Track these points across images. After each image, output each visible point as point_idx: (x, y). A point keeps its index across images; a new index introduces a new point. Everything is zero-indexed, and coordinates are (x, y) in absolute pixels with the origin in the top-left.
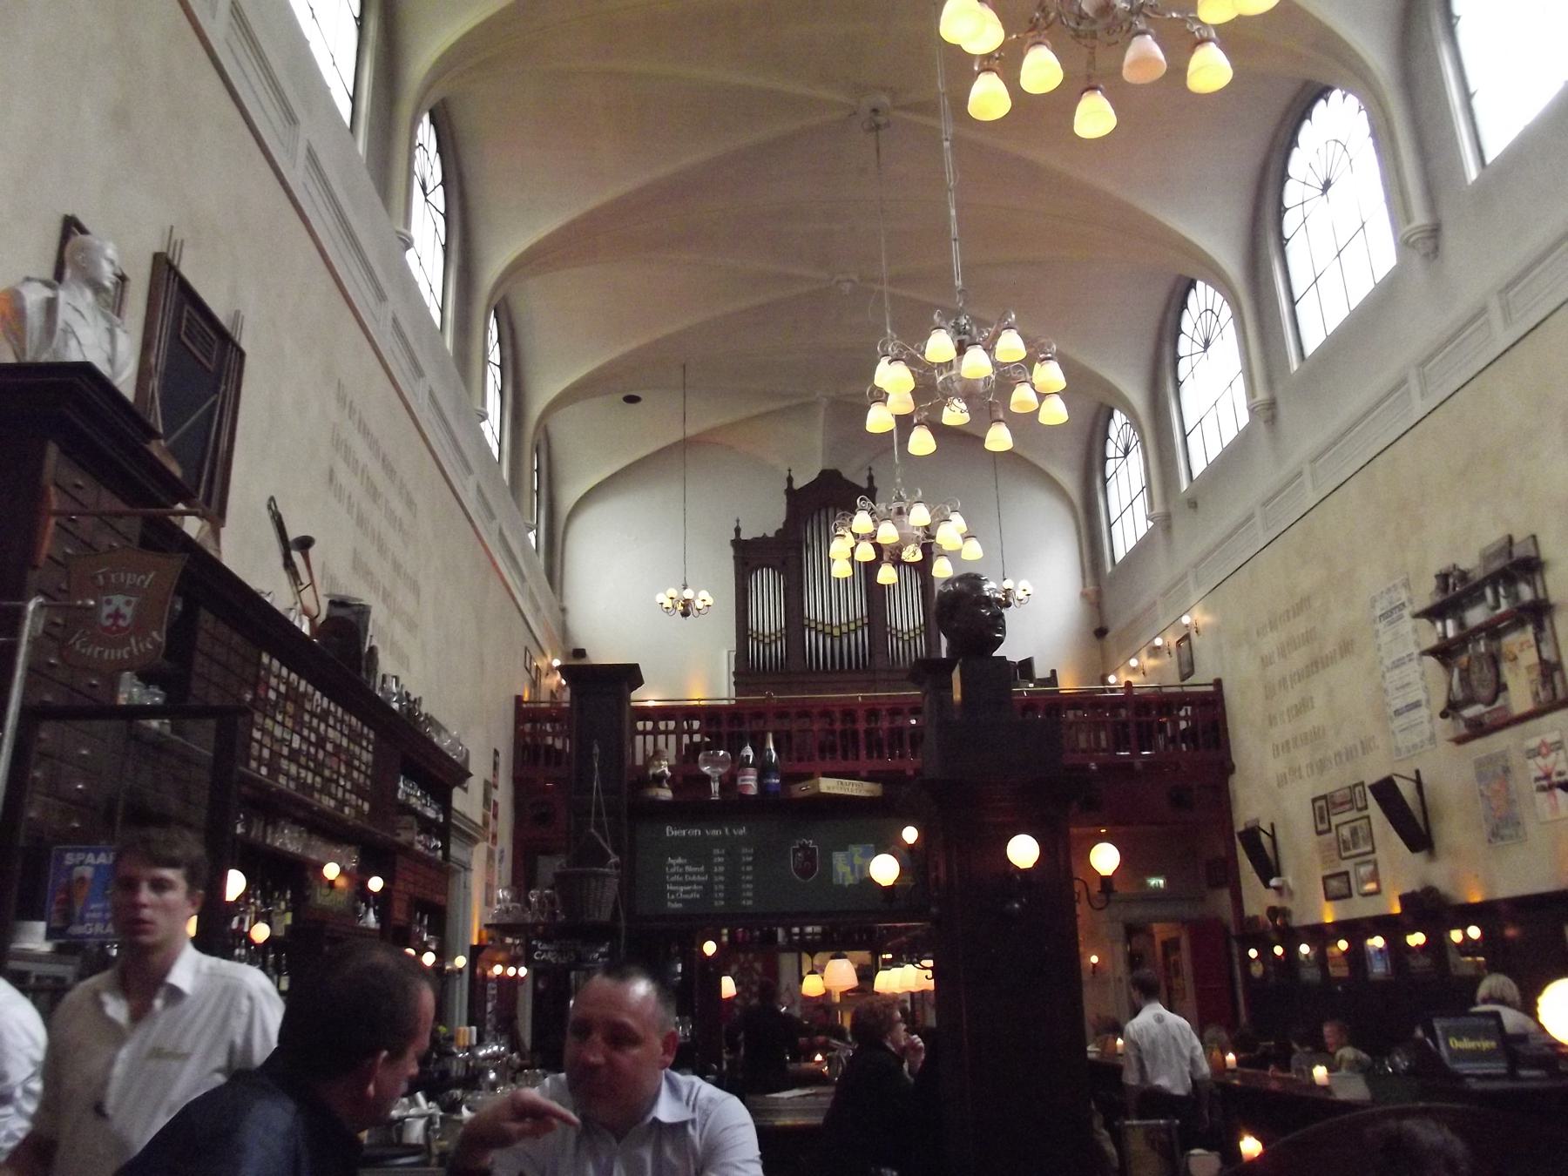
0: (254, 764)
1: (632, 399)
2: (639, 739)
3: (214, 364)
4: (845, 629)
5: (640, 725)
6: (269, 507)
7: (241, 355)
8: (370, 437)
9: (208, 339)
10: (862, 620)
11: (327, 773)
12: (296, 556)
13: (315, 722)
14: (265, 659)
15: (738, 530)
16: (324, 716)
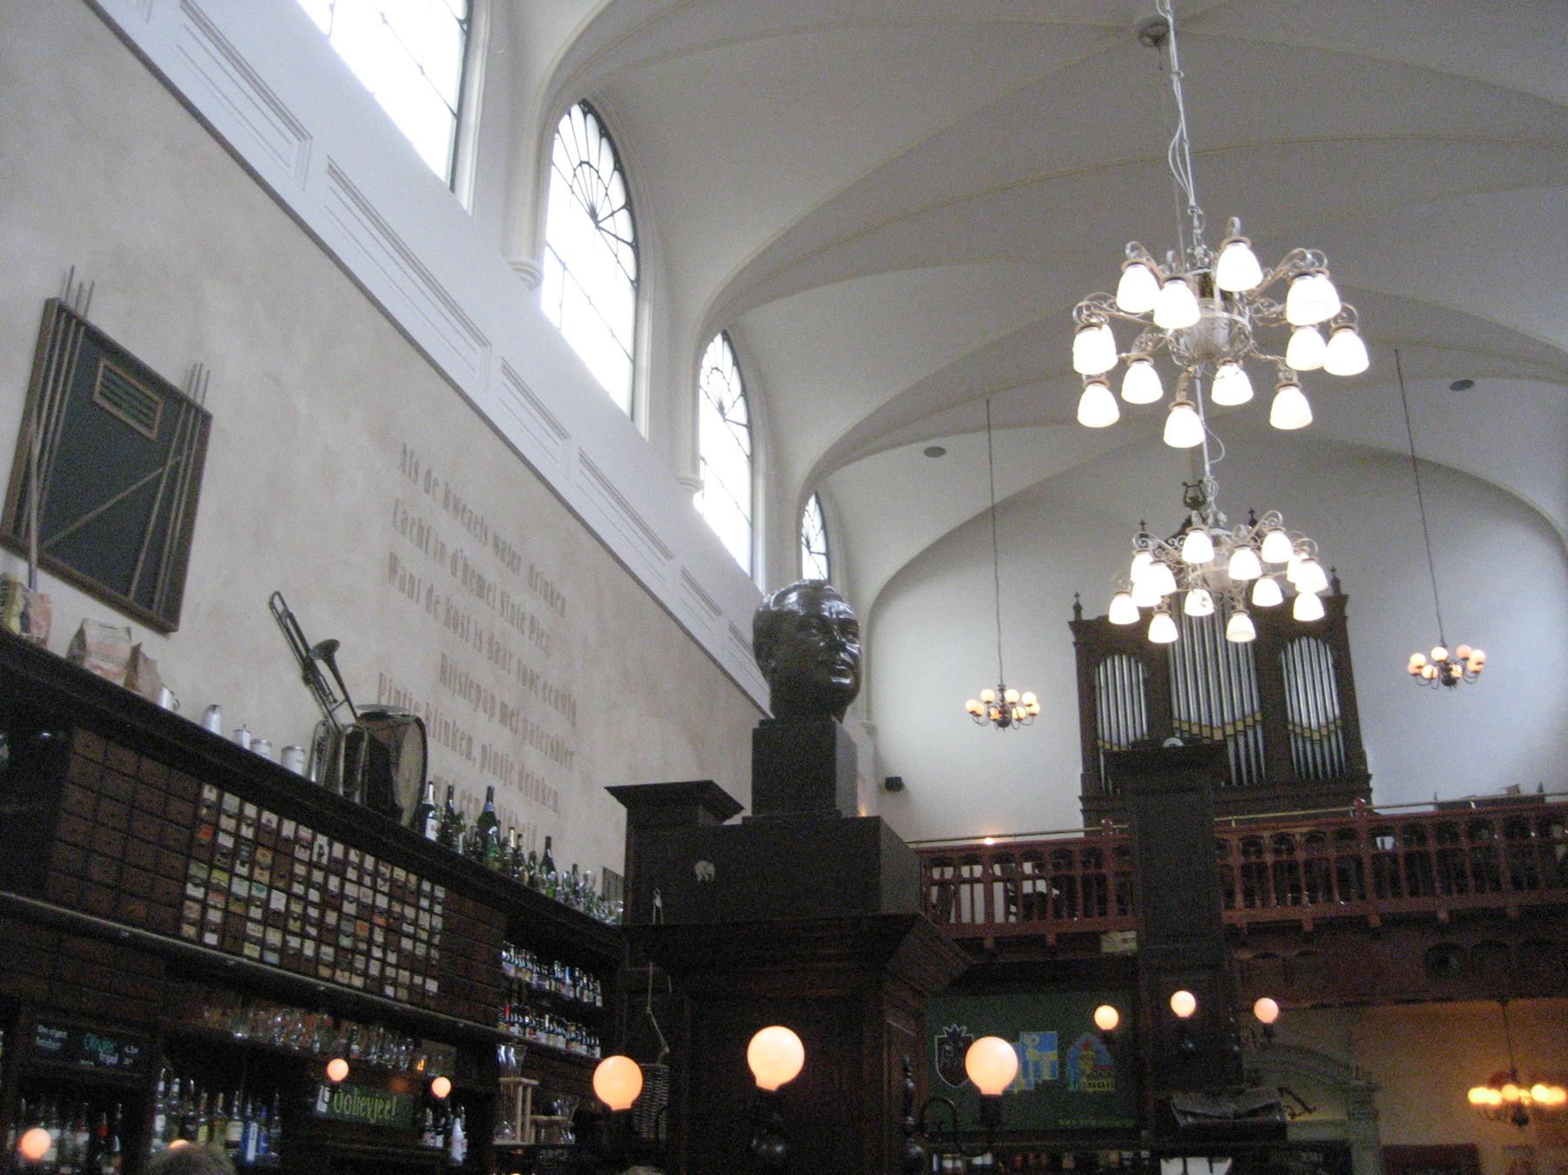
0: (189, 931)
1: (934, 452)
2: (965, 889)
3: (156, 431)
4: (1229, 730)
5: (936, 873)
6: (272, 606)
7: (206, 418)
8: (467, 516)
9: (136, 403)
10: (1244, 722)
11: (346, 942)
12: (321, 666)
13: (318, 876)
14: (210, 794)
15: (1078, 608)
16: (337, 868)
